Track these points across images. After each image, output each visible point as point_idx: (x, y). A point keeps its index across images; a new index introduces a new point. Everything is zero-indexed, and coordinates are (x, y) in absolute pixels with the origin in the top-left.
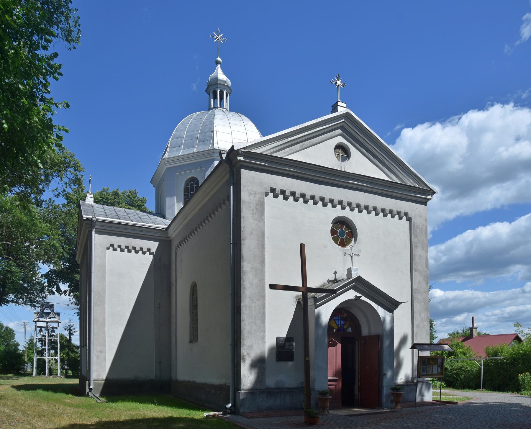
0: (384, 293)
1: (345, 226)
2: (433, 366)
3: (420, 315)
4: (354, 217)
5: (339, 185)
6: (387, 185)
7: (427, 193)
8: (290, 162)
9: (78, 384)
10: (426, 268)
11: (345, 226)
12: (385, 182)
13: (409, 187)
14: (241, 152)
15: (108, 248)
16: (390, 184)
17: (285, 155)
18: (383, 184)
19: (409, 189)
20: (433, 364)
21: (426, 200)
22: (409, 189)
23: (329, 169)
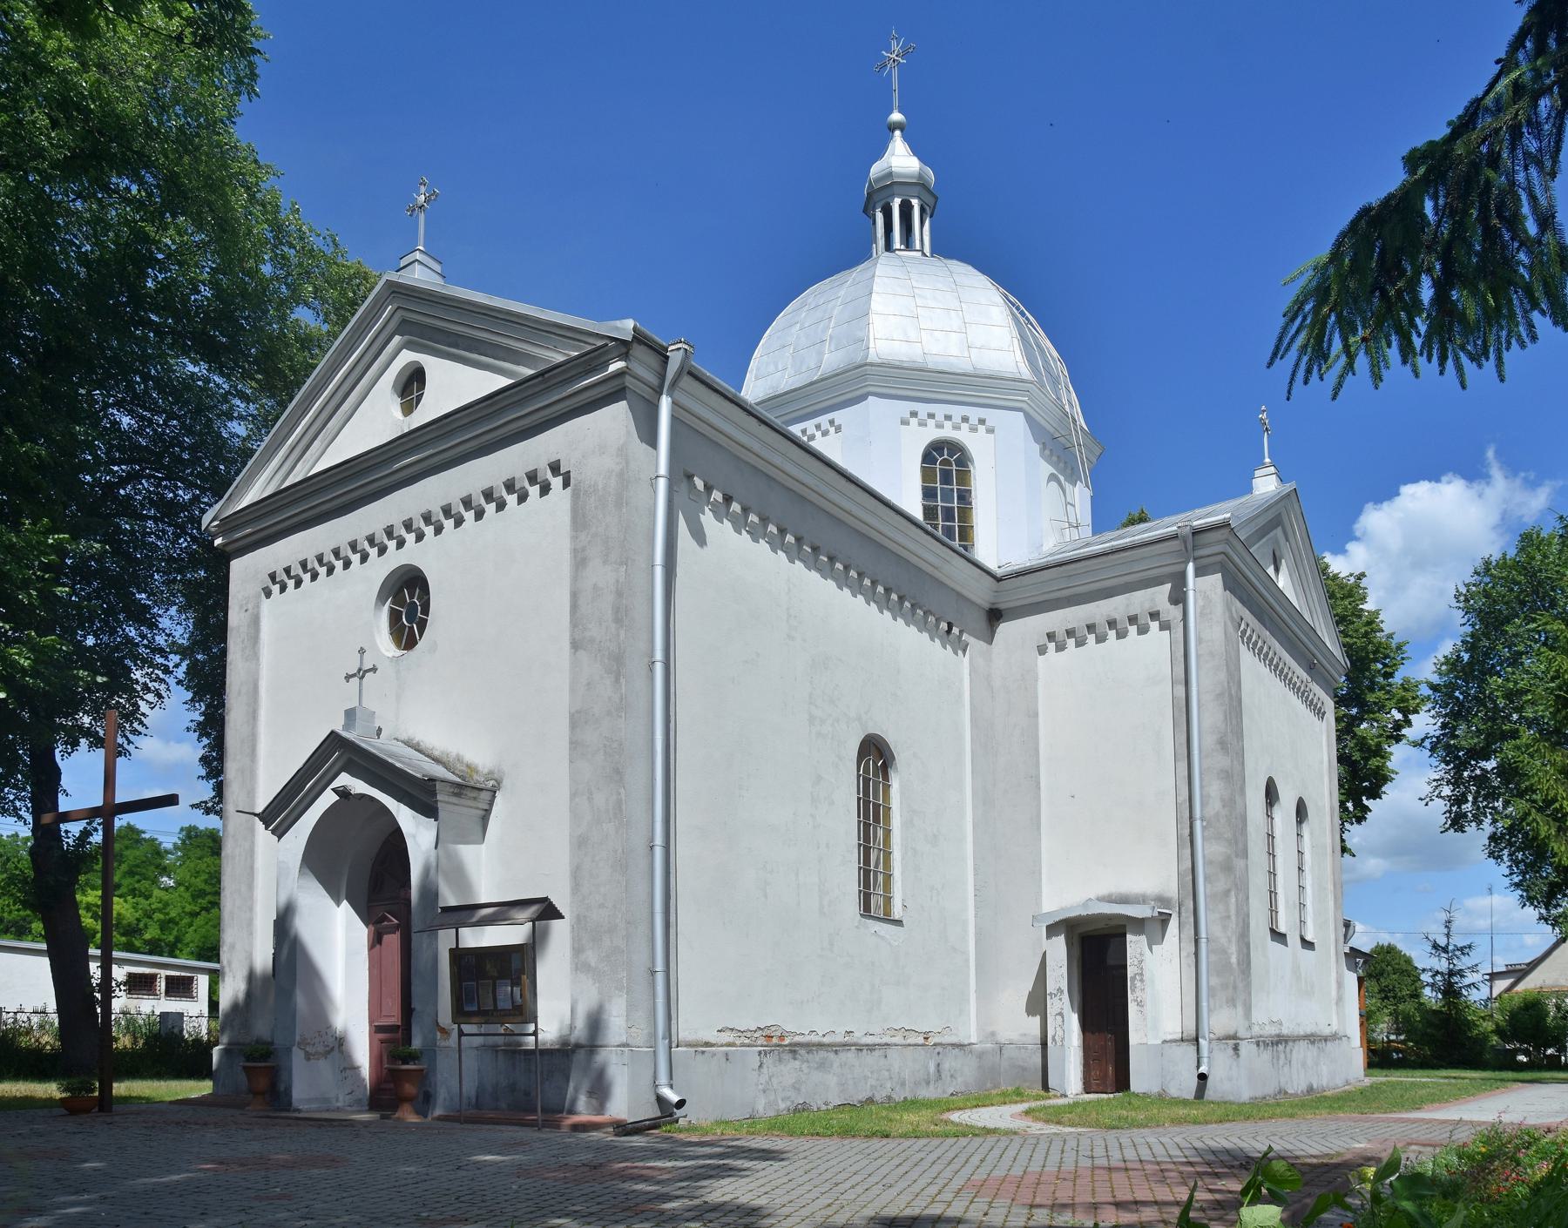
0: (283, 794)
1: (418, 590)
2: (498, 982)
3: (590, 799)
4: (412, 554)
5: (598, 399)
6: (480, 415)
7: (602, 360)
8: (520, 391)
9: (116, 1081)
10: (613, 626)
11: (418, 590)
12: (471, 410)
13: (540, 379)
14: (213, 530)
15: (1042, 650)
16: (467, 415)
17: (308, 466)
18: (519, 397)
19: (543, 386)
20: (496, 974)
21: (616, 382)
22: (543, 386)
23: (391, 446)
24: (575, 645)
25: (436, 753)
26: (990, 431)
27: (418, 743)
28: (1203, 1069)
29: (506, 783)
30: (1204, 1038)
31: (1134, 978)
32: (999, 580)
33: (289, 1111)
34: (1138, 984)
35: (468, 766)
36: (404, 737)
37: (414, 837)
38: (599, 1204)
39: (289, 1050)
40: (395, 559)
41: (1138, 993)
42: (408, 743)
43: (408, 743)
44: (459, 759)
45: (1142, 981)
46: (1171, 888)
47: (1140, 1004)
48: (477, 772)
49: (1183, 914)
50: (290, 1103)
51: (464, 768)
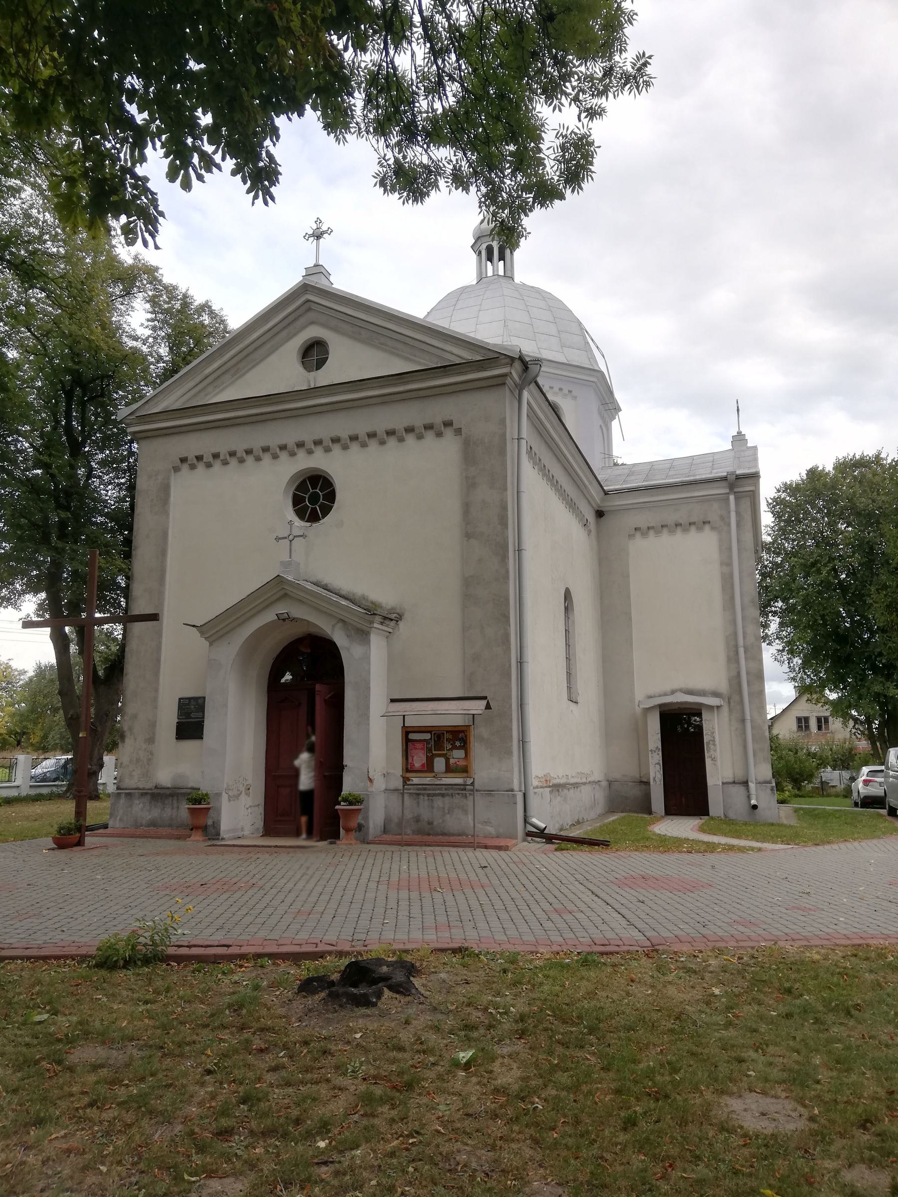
24: (468, 536)
25: (343, 593)
26: (575, 398)
27: (326, 585)
28: (753, 802)
29: (407, 616)
30: (752, 782)
31: (708, 743)
32: (606, 493)
33: (218, 839)
34: (712, 747)
35: (372, 603)
36: (314, 579)
37: (348, 649)
38: (141, 910)
39: (219, 795)
40: (304, 462)
41: (712, 752)
42: (316, 584)
43: (316, 584)
44: (364, 597)
45: (714, 745)
46: (723, 686)
47: (714, 759)
48: (381, 607)
49: (732, 704)
50: (218, 834)
51: (370, 604)
